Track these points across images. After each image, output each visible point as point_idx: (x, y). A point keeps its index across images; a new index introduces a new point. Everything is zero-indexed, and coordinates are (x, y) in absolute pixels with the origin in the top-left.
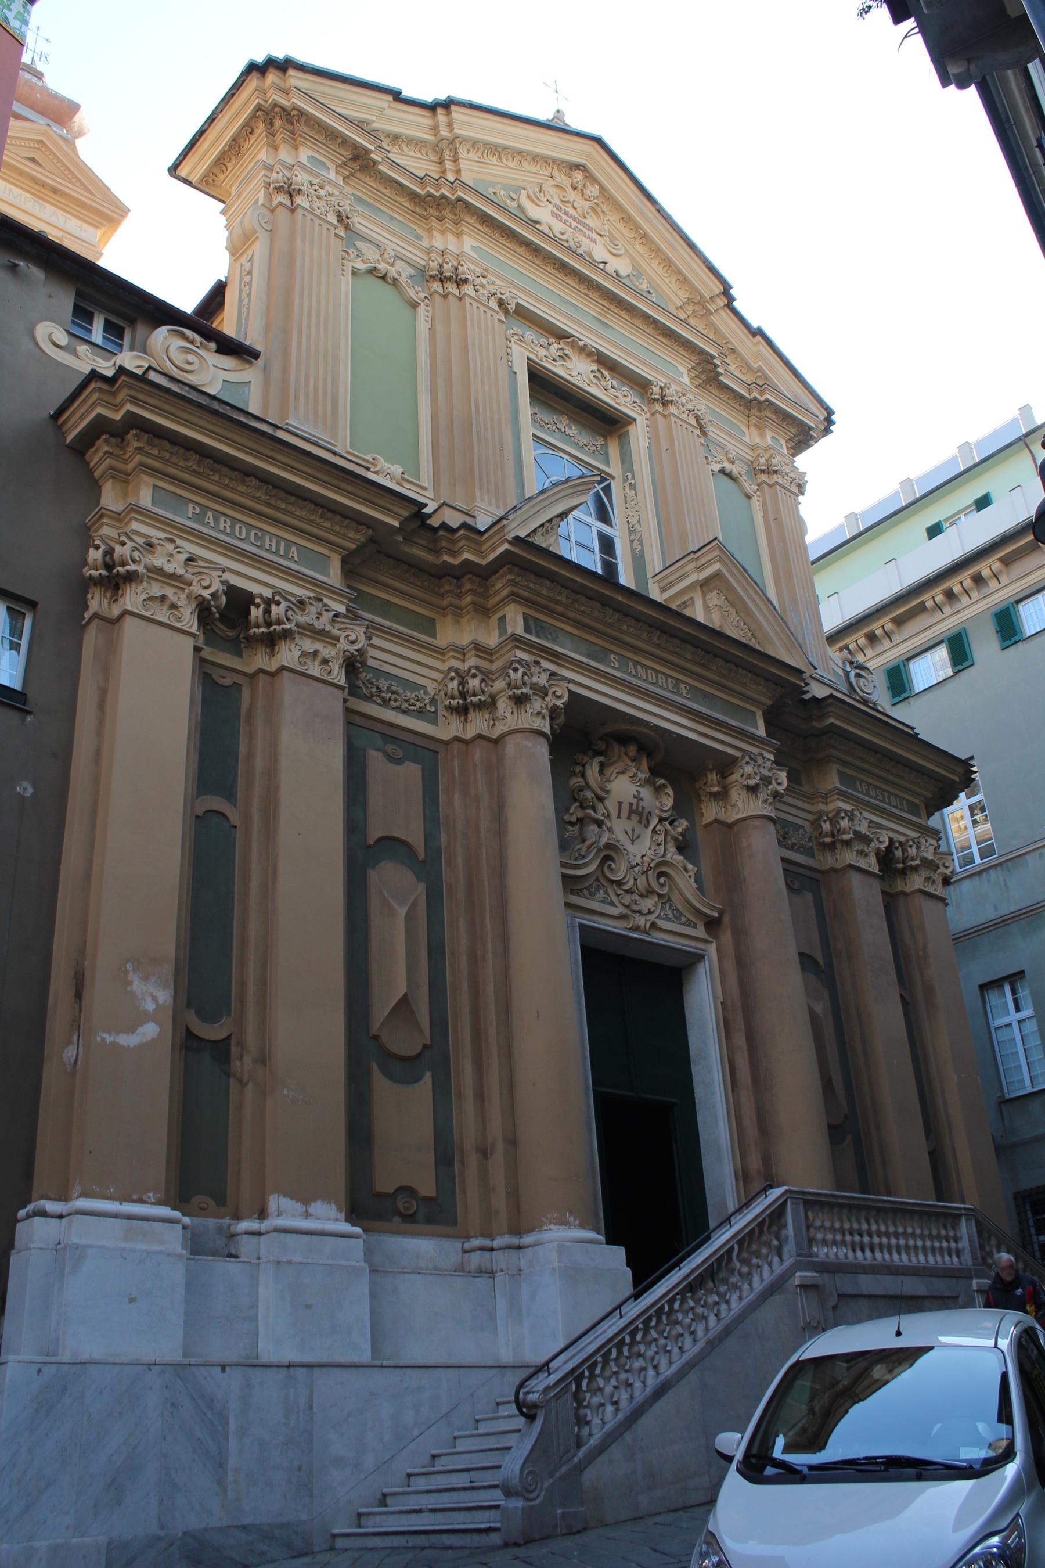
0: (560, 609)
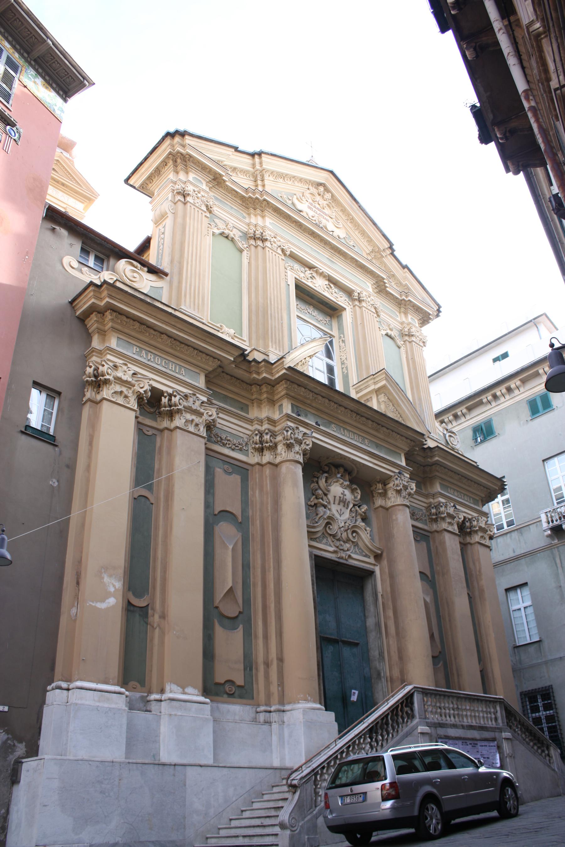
0: (309, 402)
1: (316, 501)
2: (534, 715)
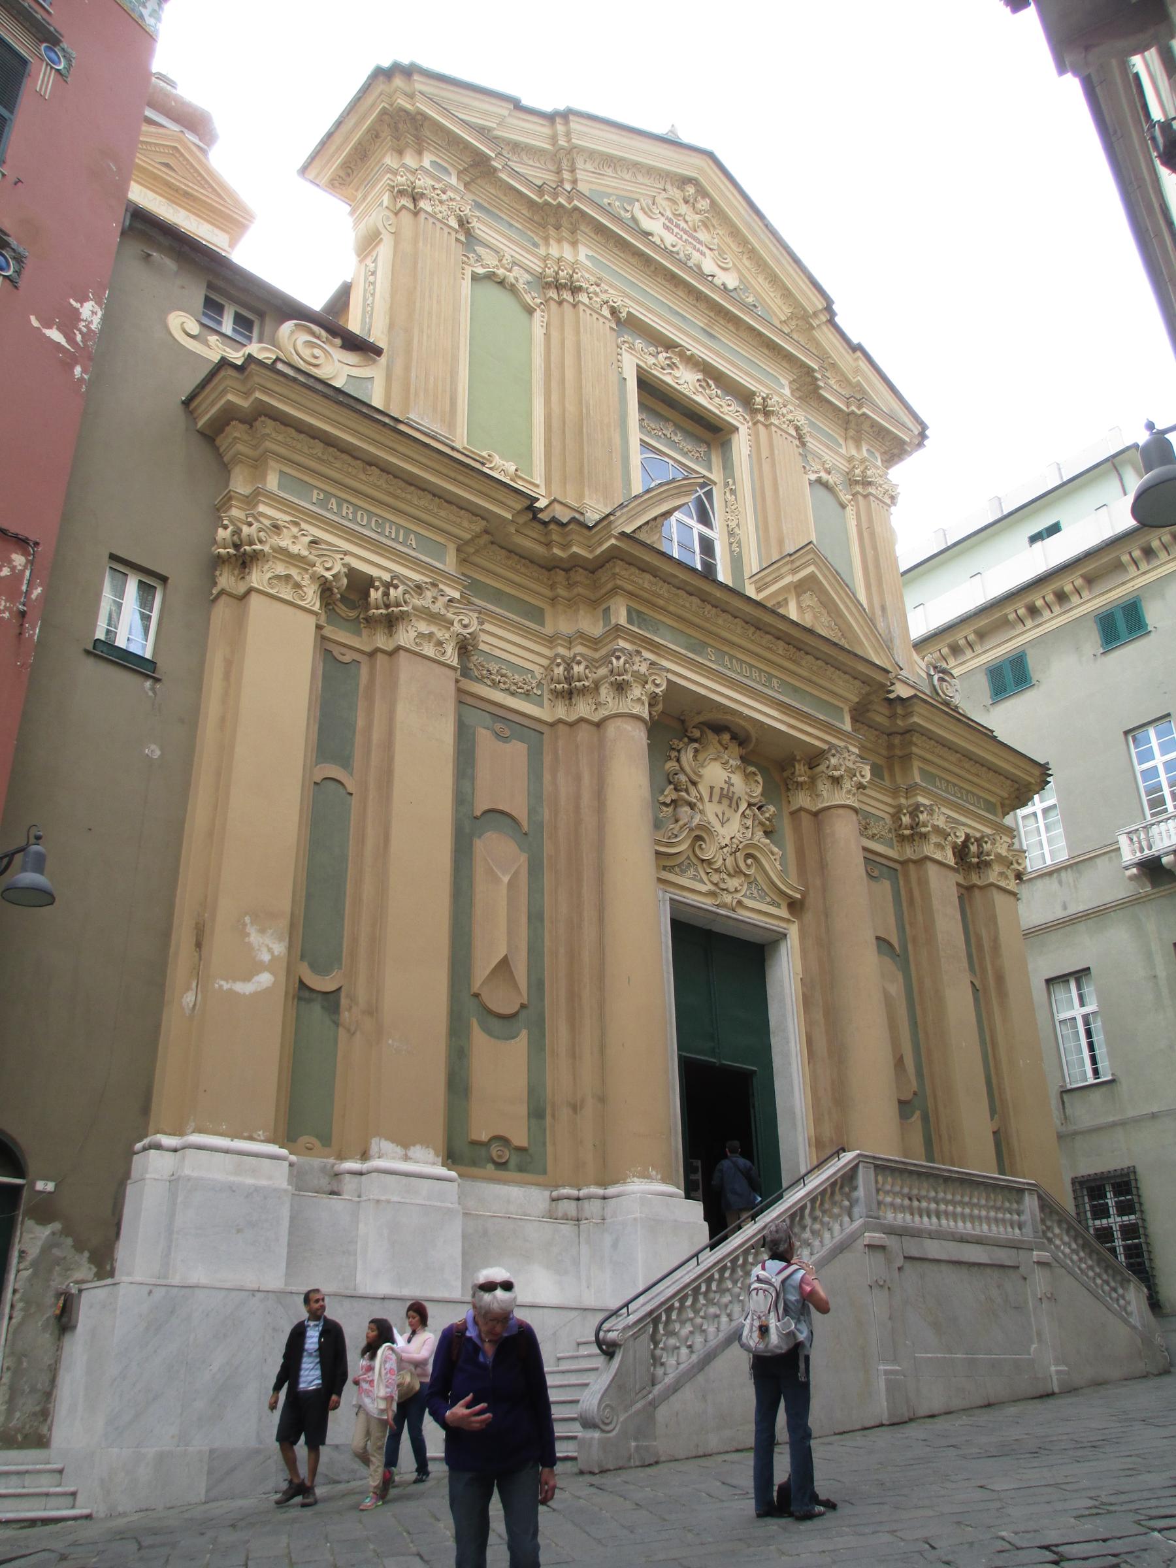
0: (661, 602)
1: (674, 796)
2: (1098, 1222)
